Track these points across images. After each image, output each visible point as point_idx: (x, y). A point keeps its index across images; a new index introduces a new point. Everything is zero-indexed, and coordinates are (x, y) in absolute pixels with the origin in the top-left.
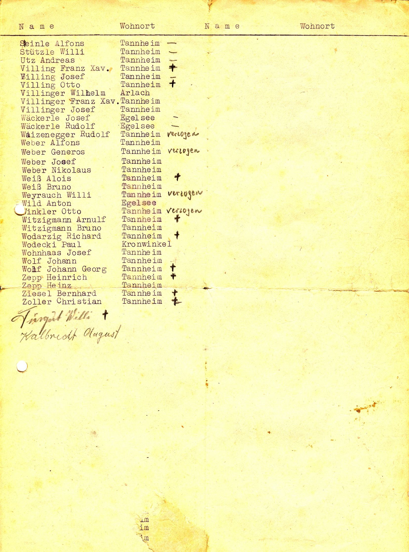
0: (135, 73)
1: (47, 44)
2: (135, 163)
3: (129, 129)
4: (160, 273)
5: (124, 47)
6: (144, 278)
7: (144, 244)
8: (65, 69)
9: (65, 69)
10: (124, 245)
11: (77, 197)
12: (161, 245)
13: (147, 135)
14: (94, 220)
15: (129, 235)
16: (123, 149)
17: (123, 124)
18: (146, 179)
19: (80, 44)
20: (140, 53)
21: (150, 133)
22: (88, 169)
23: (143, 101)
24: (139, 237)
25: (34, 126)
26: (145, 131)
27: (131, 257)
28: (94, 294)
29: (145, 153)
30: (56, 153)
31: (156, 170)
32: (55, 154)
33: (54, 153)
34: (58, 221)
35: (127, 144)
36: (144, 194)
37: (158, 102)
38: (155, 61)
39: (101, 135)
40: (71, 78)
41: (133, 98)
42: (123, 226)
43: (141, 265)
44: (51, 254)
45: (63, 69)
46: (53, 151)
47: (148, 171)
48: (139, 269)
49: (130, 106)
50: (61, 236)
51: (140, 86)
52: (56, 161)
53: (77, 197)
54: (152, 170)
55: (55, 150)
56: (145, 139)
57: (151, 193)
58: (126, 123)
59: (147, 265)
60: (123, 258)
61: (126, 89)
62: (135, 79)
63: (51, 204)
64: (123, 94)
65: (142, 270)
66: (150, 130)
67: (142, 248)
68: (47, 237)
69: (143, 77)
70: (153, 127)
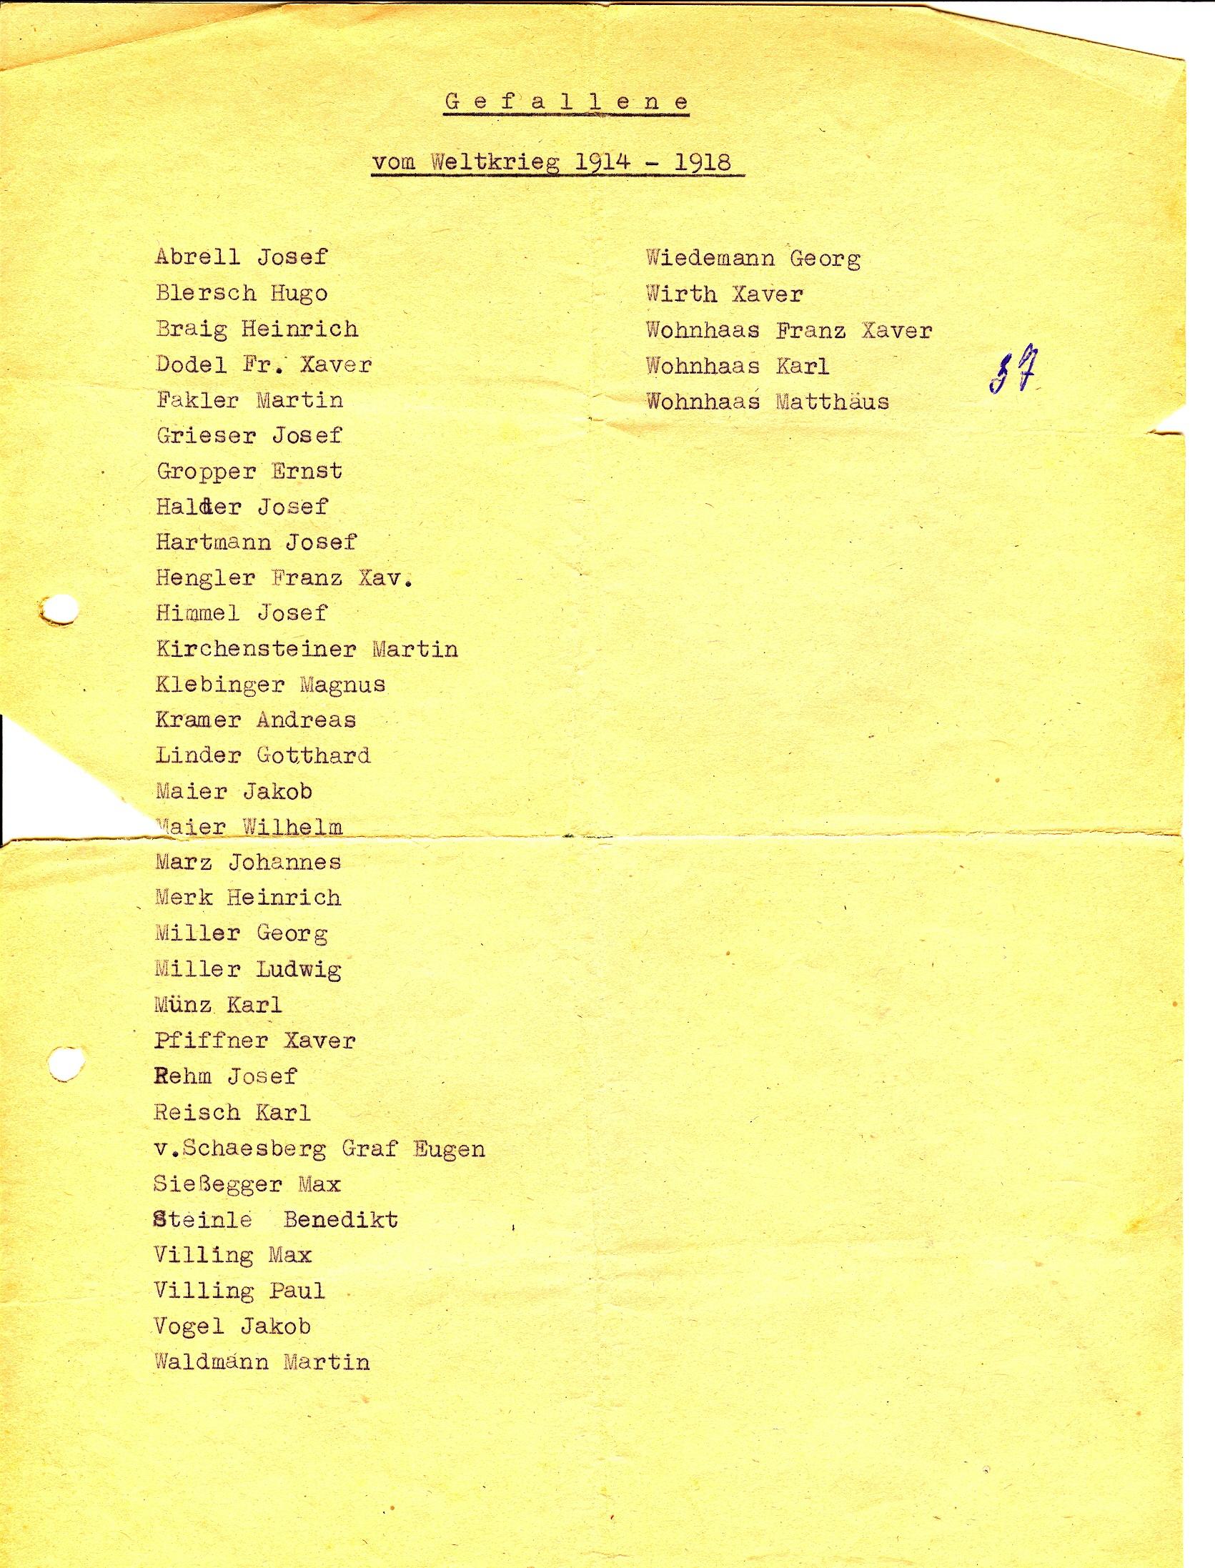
11: (196, 1297)
14: (305, 1292)
19: (257, 651)
22: (752, 365)
25: (237, 291)
30: (803, 262)
32: (267, 937)
33: (263, 936)
34: (723, 370)
44: (731, 370)
45: (783, 333)
46: (797, 255)
50: (859, 257)
53: (196, 1297)
55: (800, 252)
63: (270, 721)
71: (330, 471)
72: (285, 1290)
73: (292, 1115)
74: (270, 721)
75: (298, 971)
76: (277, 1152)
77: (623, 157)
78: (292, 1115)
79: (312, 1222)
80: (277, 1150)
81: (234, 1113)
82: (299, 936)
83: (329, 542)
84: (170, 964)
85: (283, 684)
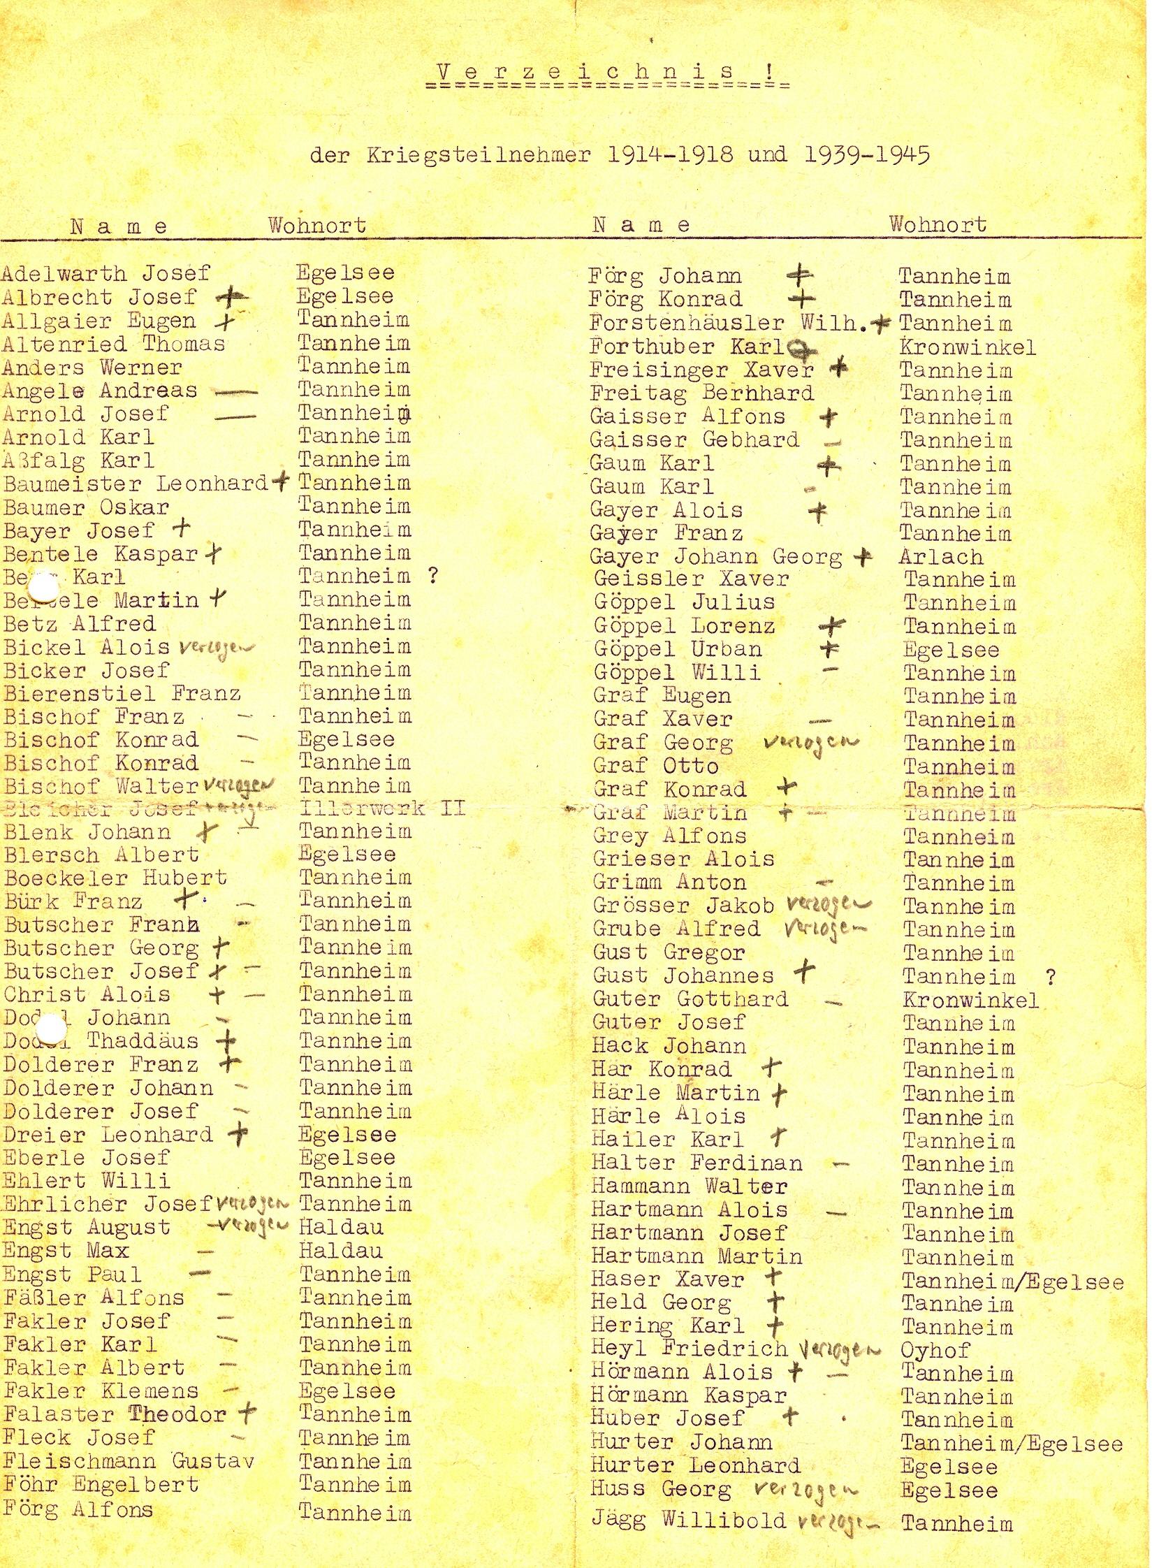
2: (942, 749)
5: (915, 1198)
6: (964, 1422)
7: (962, 349)
8: (688, 534)
9: (688, 534)
15: (923, 1045)
16: (909, 1251)
23: (967, 745)
24: (951, 1073)
27: (927, 1387)
28: (792, 441)
29: (971, 680)
36: (967, 1046)
37: (1010, 582)
38: (999, 886)
40: (748, 1238)
41: (937, 570)
48: (948, 466)
52: (676, 1043)
56: (969, 478)
61: (915, 546)
62: (943, 1078)
64: (905, 559)
65: (956, 374)
69: (963, 371)
70: (994, 654)
72: (102, 1274)
73: (695, 465)
74: (16, 393)
77: (909, 150)
78: (695, 465)
79: (748, 628)
80: (626, 1419)
81: (849, 324)
82: (704, 1305)
85: (112, 1110)
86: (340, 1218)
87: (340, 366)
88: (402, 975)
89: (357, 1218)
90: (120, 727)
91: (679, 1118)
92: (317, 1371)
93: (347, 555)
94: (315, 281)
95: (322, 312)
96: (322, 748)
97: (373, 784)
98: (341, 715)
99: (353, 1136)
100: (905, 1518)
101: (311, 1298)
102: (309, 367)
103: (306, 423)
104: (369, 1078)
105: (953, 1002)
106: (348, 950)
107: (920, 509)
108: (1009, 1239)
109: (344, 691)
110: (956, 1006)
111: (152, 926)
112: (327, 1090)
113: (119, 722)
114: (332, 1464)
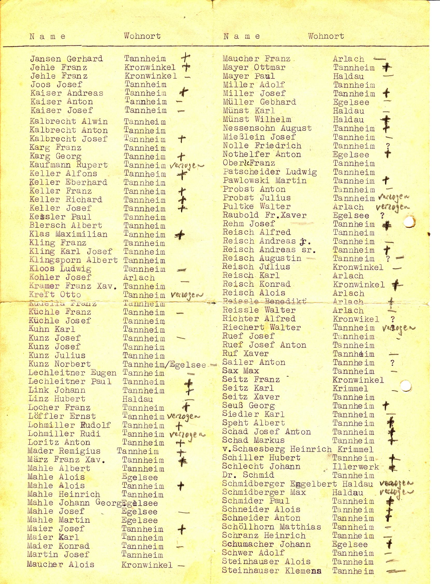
0: (137, 465)
1: (48, 235)
3: (130, 523)
4: (163, 335)
10: (127, 77)
12: (166, 68)
13: (149, 530)
17: (124, 518)
18: (151, 112)
20: (145, 149)
21: (153, 528)
24: (140, 539)
26: (148, 525)
31: (159, 313)
35: (129, 487)
39: (102, 426)
42: (124, 483)
43: (144, 89)
47: (152, 158)
49: (132, 335)
51: (144, 270)
54: (155, 313)
57: (154, 372)
58: (128, 517)
59: (150, 205)
60: (125, 120)
61: (129, 274)
66: (152, 525)
67: (146, 79)
68: (44, 460)
71: (249, 198)
73: (68, 330)
75: (302, 172)
76: (241, 190)
78: (131, 278)
83: (79, 555)
84: (228, 92)
86: (138, 396)
87: (139, 217)
88: (162, 228)
89: (144, 396)
90: (63, 247)
91: (260, 364)
92: (131, 193)
93: (142, 183)
94: (129, 523)
95: (131, 526)
96: (131, 523)
97: (151, 182)
98: (140, 174)
99: (142, 504)
100: (334, 568)
101: (127, 373)
102: (128, 165)
103: (126, 264)
104: (149, 361)
105: (351, 381)
106: (142, 175)
107: (341, 171)
108: (372, 460)
109: (141, 208)
110: (352, 382)
111: (69, 243)
112: (134, 122)
113: (67, 313)
114: (135, 357)
